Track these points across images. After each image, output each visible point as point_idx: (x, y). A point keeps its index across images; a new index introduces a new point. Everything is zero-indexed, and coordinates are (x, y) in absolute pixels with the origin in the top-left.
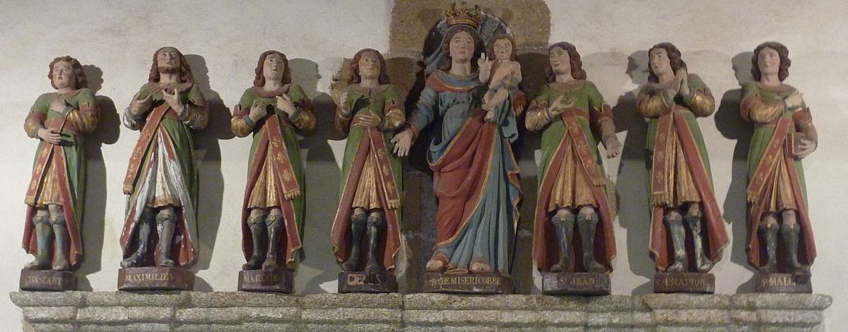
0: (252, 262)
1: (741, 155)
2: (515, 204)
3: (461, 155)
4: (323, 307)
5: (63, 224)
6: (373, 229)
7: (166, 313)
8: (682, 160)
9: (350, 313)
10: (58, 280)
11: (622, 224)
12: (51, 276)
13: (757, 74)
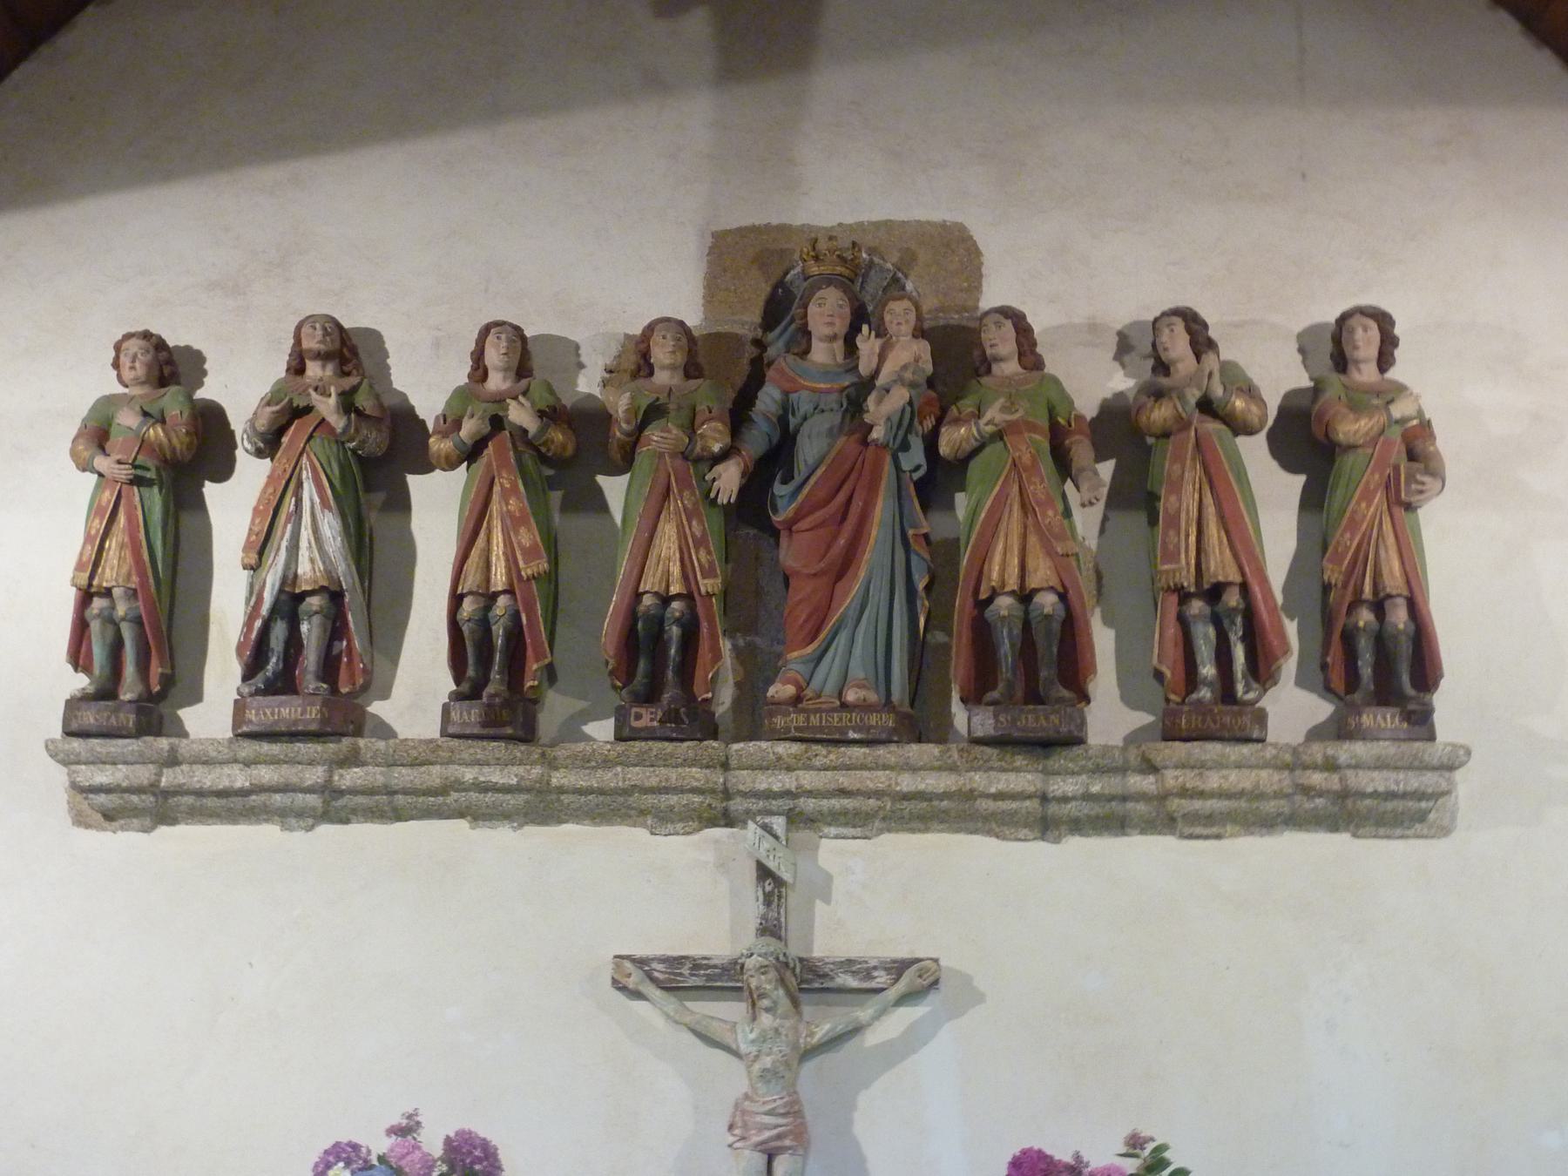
0: (465, 687)
4: (588, 765)
6: (675, 631)
7: (315, 775)
8: (1210, 511)
9: (636, 775)
10: (129, 719)
11: (1108, 621)
12: (116, 711)
13: (1341, 362)
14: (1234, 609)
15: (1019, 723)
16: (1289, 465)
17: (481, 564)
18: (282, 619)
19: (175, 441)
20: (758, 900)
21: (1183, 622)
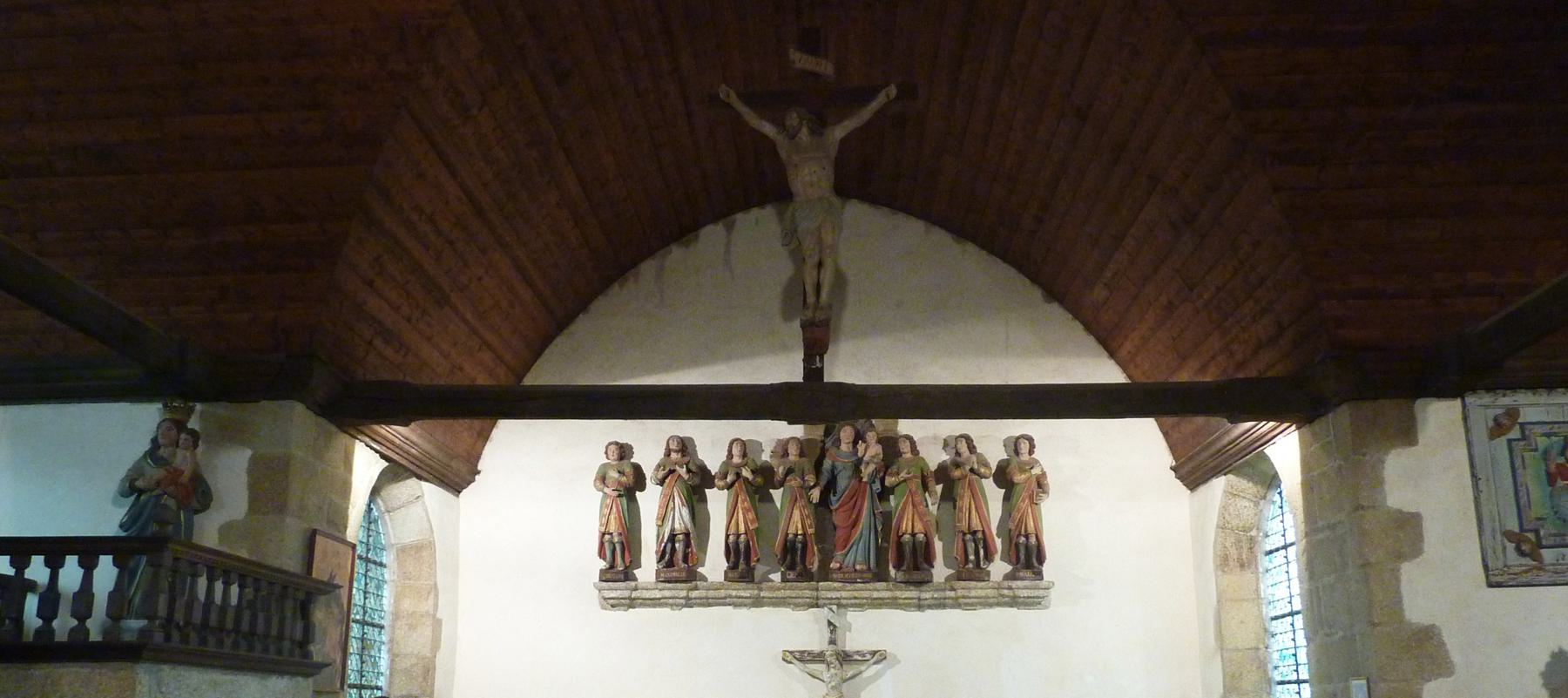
0: (731, 565)
1: (1007, 498)
2: (879, 529)
3: (849, 502)
5: (622, 543)
6: (800, 545)
7: (683, 593)
8: (973, 506)
9: (788, 593)
10: (622, 577)
11: (940, 539)
13: (1017, 452)
14: (980, 539)
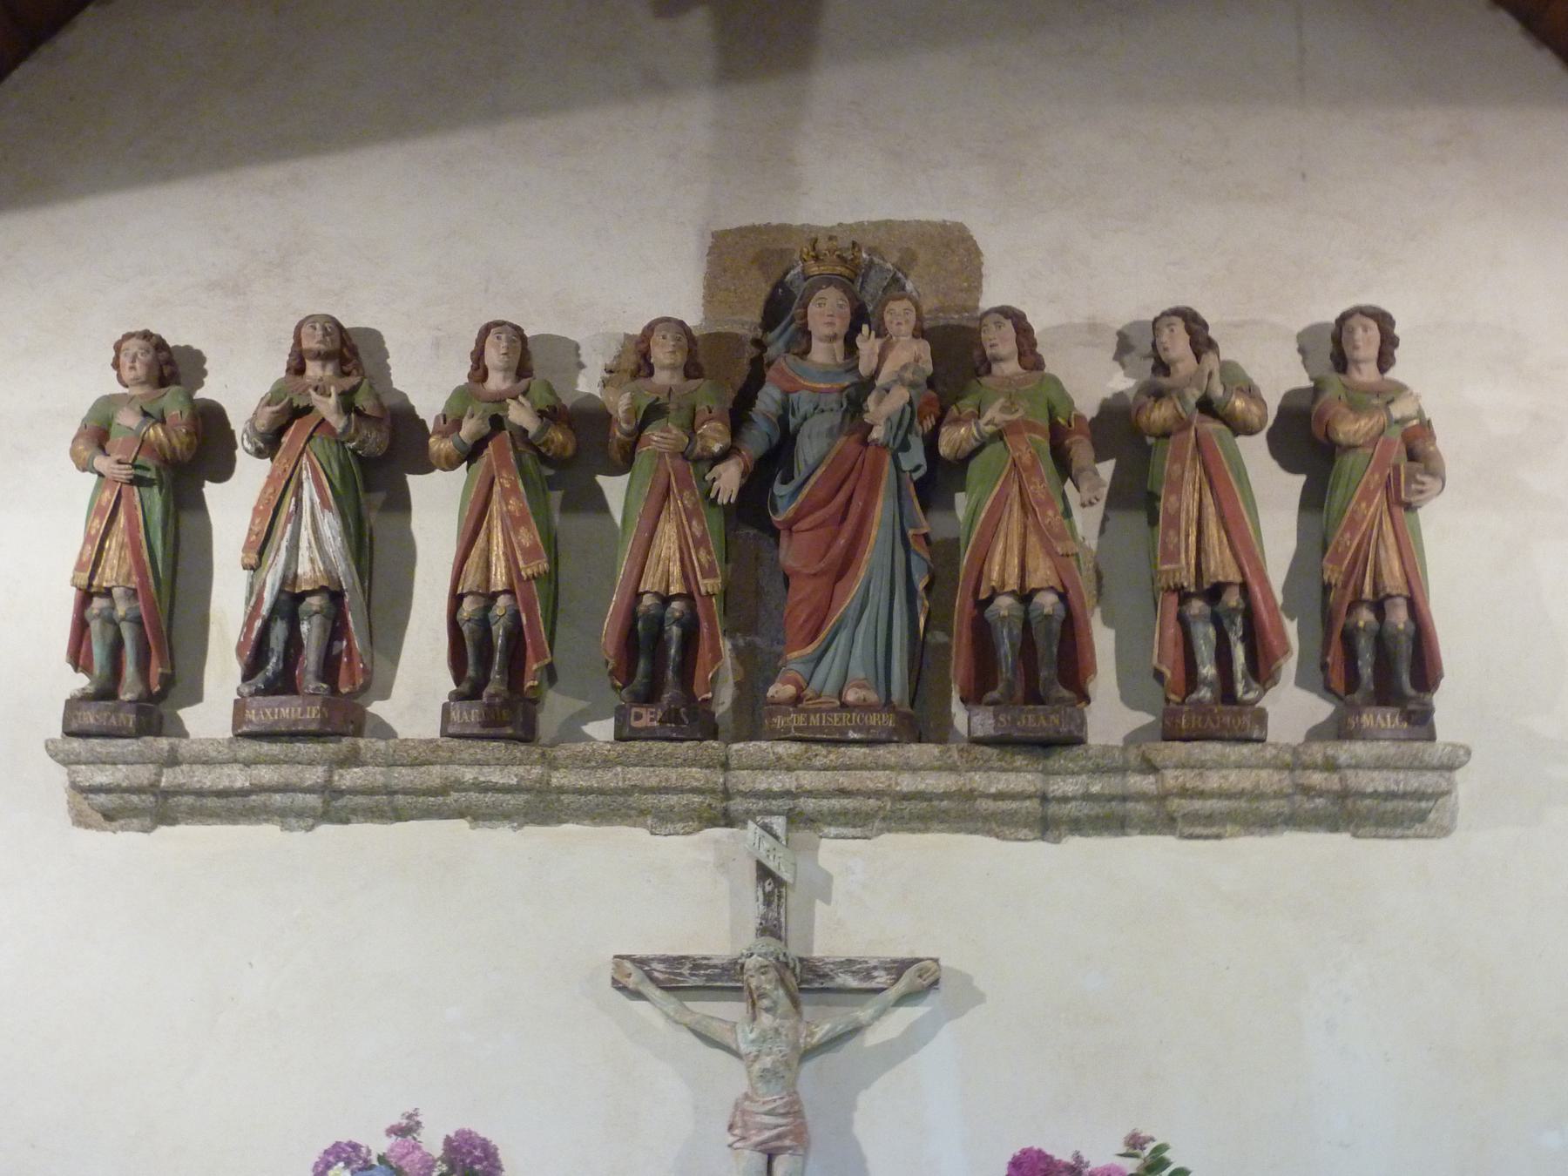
0: (465, 687)
4: (588, 765)
5: (138, 621)
6: (675, 631)
7: (315, 775)
8: (1210, 511)
9: (636, 775)
10: (129, 719)
11: (1108, 621)
12: (116, 711)
13: (1341, 362)
14: (1234, 609)
15: (1019, 723)
16: (1289, 465)
17: (481, 564)
18: (282, 619)
19: (175, 441)
20: (758, 900)
21: (1183, 622)
